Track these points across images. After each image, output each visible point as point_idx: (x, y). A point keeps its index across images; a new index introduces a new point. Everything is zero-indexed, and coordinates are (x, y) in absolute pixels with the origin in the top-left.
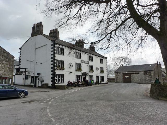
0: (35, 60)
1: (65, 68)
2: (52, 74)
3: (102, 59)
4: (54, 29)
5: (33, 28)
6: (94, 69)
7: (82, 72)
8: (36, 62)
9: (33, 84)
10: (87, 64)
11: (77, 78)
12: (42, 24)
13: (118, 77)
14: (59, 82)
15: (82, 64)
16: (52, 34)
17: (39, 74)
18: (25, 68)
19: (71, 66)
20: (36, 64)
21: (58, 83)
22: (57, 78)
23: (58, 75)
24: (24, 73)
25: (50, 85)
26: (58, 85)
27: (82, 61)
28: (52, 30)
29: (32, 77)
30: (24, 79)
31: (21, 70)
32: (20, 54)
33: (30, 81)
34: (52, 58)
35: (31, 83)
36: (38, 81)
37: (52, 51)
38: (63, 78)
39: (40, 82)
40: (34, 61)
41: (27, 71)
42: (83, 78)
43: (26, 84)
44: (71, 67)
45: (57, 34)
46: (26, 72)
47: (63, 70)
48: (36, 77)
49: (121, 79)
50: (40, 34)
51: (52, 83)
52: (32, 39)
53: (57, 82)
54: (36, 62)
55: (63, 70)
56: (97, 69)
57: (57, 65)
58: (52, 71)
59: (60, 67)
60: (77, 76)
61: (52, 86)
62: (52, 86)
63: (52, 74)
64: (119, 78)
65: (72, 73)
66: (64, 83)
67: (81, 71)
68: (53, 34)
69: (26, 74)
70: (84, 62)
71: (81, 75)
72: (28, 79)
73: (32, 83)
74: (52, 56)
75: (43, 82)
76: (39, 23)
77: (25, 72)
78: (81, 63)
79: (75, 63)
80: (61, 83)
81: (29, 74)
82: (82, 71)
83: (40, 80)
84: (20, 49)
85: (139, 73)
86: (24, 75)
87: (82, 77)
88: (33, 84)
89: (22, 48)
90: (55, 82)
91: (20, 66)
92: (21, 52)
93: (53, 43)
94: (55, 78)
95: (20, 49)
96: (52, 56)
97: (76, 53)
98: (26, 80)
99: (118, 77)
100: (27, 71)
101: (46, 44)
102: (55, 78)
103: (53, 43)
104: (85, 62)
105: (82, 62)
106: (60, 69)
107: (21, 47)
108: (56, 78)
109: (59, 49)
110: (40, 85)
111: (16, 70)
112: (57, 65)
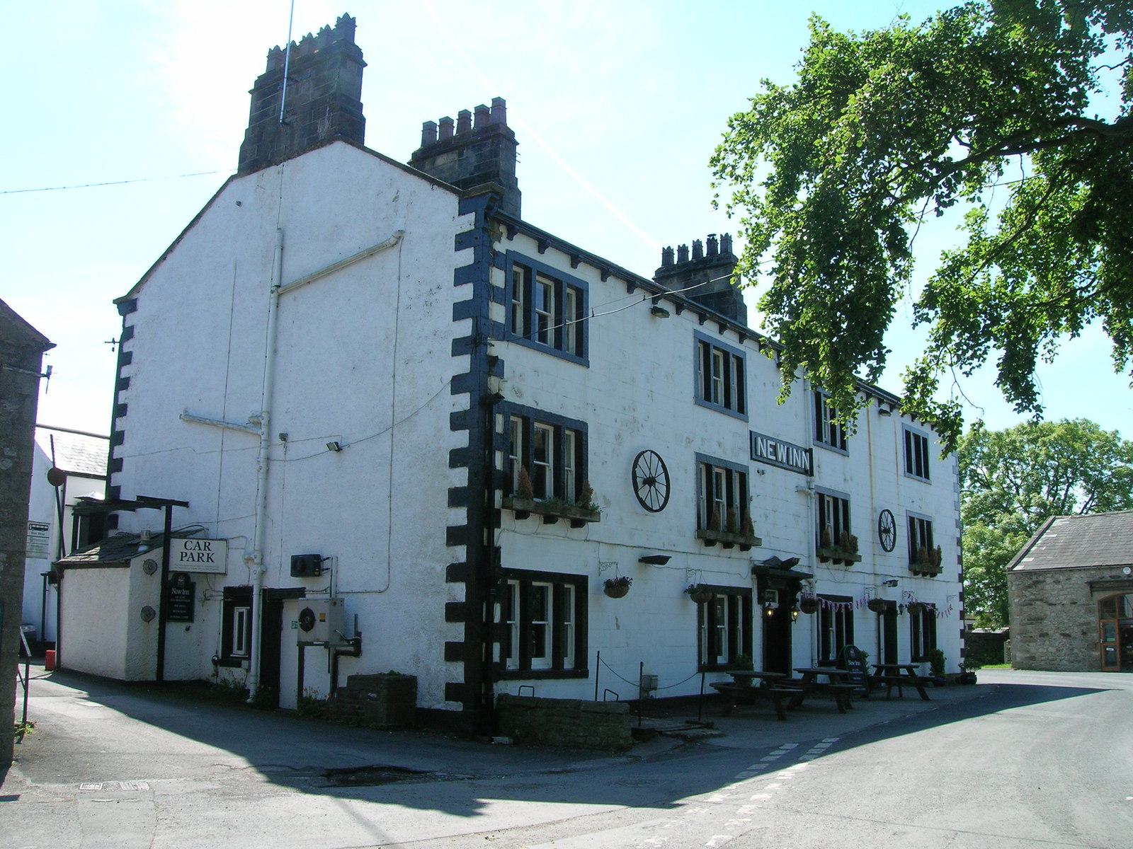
0: (270, 413)
1: (596, 500)
2: (454, 573)
3: (917, 437)
4: (464, 116)
5: (264, 91)
6: (861, 527)
7: (759, 555)
8: (278, 430)
9: (248, 676)
10: (801, 480)
11: (705, 626)
12: (361, 101)
13: (1039, 619)
14: (537, 664)
15: (754, 467)
16: (441, 160)
17: (308, 565)
18: (168, 504)
19: (650, 481)
20: (278, 451)
21: (525, 672)
22: (516, 622)
23: (526, 576)
24: (157, 554)
25: (432, 697)
26: (527, 693)
27: (753, 437)
28: (446, 122)
29: (237, 596)
30: (147, 614)
31: (131, 522)
32: (125, 359)
33: (213, 644)
34: (458, 384)
35: (226, 659)
36: (301, 646)
37: (460, 311)
38: (571, 624)
39: (317, 660)
40: (260, 424)
41: (184, 535)
42: (765, 618)
43: (171, 673)
44: (653, 496)
45: (502, 155)
46: (177, 545)
47: (577, 533)
48: (275, 601)
49: (1076, 631)
50: (330, 140)
51: (457, 672)
52: (247, 201)
53: (513, 663)
54: (284, 437)
55: (577, 524)
56: (884, 531)
57: (518, 467)
58: (454, 536)
59: (540, 491)
60: (703, 595)
61: (457, 706)
62: (457, 706)
63: (454, 573)
64: (1048, 626)
65: (662, 560)
66: (580, 671)
67: (745, 548)
68: (453, 156)
69: (176, 564)
70: (775, 453)
71: (746, 593)
72: (187, 614)
73: (237, 663)
74: (463, 364)
75: (357, 653)
76: (326, 32)
77: (164, 539)
78: (743, 458)
79: (694, 456)
80: (556, 672)
81: (202, 566)
82: (758, 542)
83: (321, 630)
84: (127, 305)
85: (1031, 605)
86: (150, 568)
87: (757, 610)
88: (248, 676)
89: (143, 300)
90: (496, 657)
91: (117, 479)
92: (128, 333)
93: (471, 217)
94: (497, 619)
95: (127, 305)
96: (463, 364)
97: (705, 346)
98: (174, 629)
99: (1039, 619)
100: (184, 535)
101: (400, 236)
102: (497, 619)
103: (471, 217)
104: (782, 452)
105: (755, 455)
106: (549, 519)
107: (137, 288)
108: (507, 614)
109: (539, 283)
110: (318, 683)
111: (76, 516)
112: (518, 467)
